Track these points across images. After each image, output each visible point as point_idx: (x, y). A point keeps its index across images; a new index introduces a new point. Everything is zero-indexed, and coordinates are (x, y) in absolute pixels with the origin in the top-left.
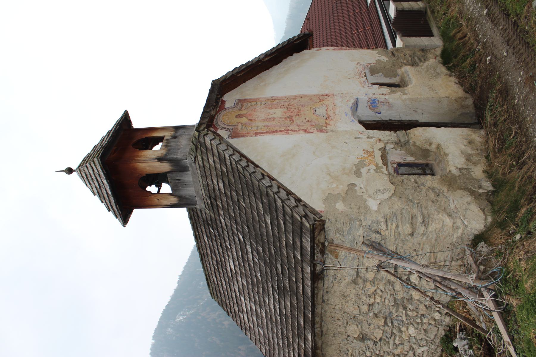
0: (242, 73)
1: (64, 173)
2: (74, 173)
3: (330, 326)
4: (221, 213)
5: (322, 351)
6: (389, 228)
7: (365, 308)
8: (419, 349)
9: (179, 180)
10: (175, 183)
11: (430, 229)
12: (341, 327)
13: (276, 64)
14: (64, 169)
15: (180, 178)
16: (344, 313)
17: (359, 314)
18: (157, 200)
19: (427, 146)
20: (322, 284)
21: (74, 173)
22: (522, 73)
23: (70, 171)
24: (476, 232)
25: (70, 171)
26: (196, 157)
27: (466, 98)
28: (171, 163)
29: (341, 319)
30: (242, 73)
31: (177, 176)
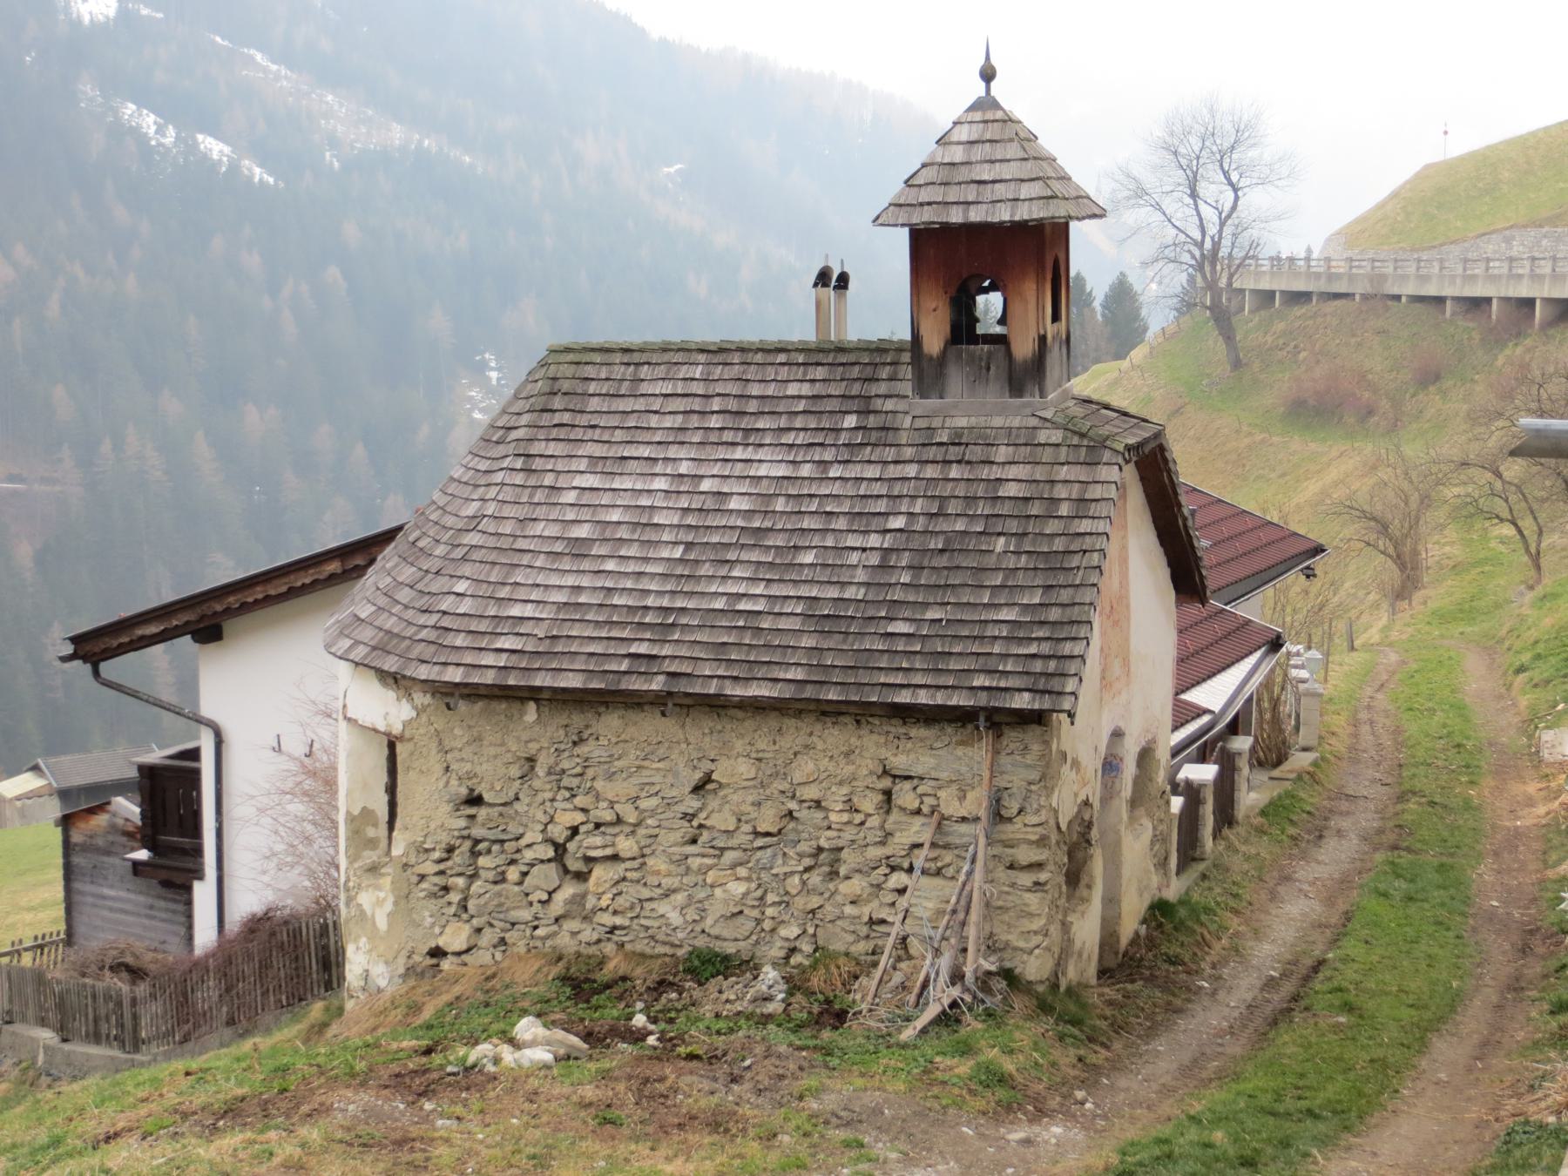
0: (1167, 481)
1: (982, 61)
2: (983, 84)
3: (747, 723)
4: (931, 472)
5: (652, 703)
6: (1029, 829)
7: (811, 793)
8: (675, 908)
9: (988, 369)
10: (981, 359)
11: (1027, 895)
12: (749, 748)
13: (1159, 536)
14: (994, 61)
15: (993, 368)
16: (795, 754)
17: (795, 782)
18: (934, 306)
19: (1083, 883)
20: (879, 713)
21: (979, 89)
22: (1105, 1081)
23: (988, 75)
24: (1017, 971)
25: (988, 75)
26: (1056, 426)
27: (1116, 953)
28: (1033, 361)
29: (777, 747)
30: (1167, 481)
31: (998, 367)
